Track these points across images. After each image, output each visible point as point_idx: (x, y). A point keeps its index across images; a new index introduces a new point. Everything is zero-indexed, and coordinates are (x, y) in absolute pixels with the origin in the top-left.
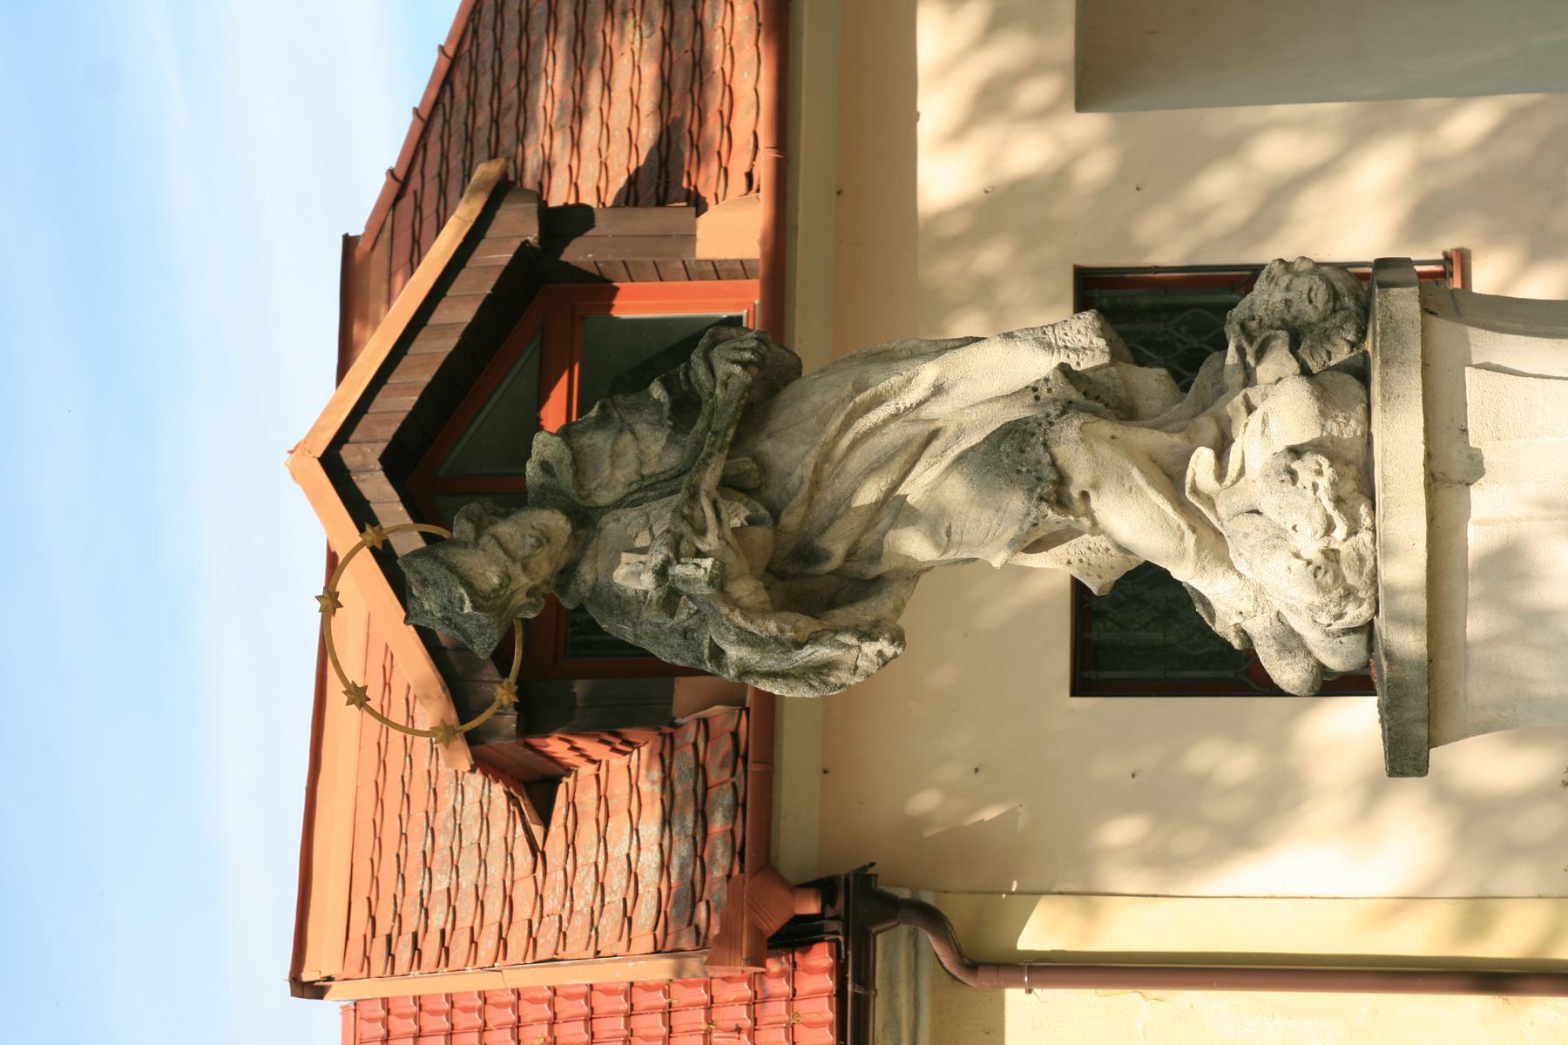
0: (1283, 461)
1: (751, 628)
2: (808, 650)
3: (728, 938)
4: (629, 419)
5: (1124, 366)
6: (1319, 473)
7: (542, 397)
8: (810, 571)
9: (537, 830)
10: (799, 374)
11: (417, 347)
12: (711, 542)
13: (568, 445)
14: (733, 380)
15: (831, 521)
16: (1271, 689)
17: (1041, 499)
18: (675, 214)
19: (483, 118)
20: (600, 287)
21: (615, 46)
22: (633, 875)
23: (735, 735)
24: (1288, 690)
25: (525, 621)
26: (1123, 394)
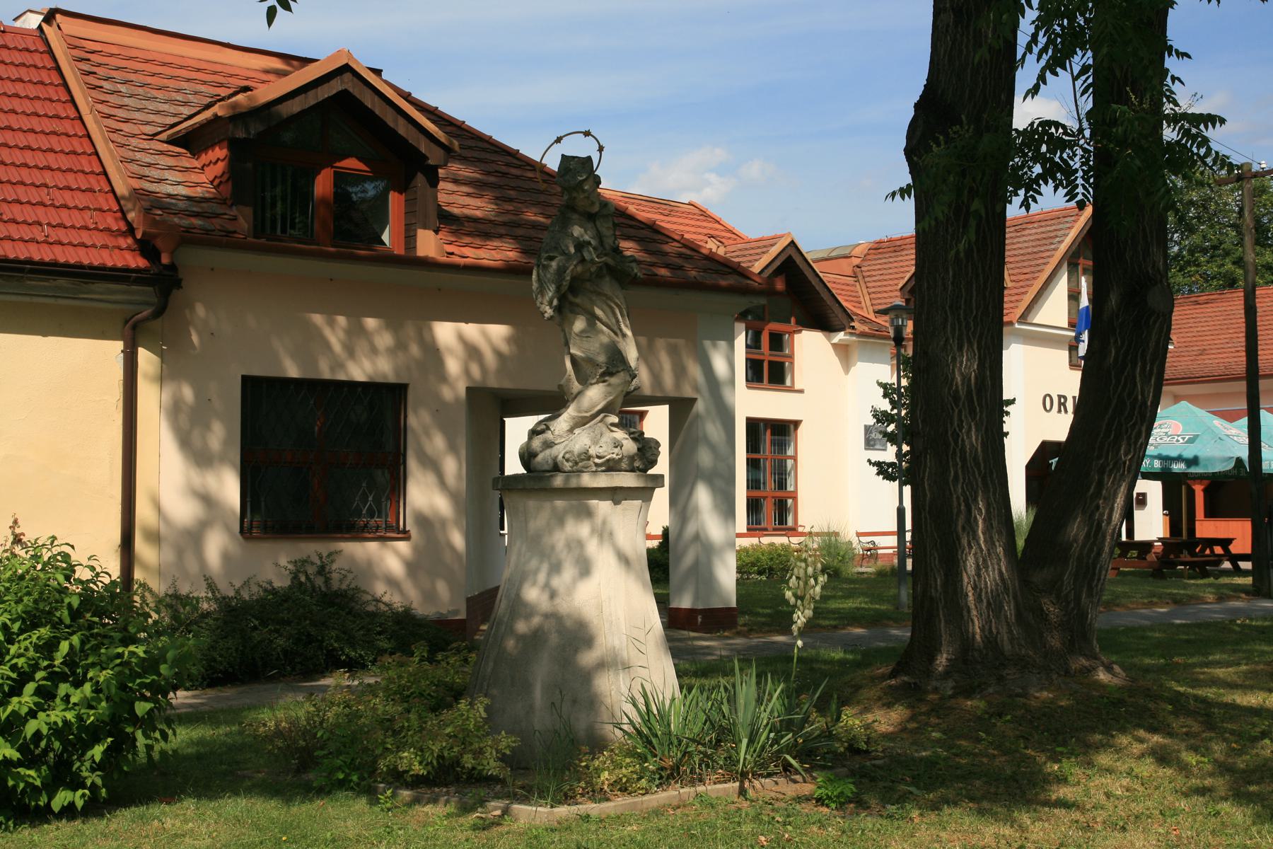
7: (360, 159)
22: (160, 181)
23: (235, 232)
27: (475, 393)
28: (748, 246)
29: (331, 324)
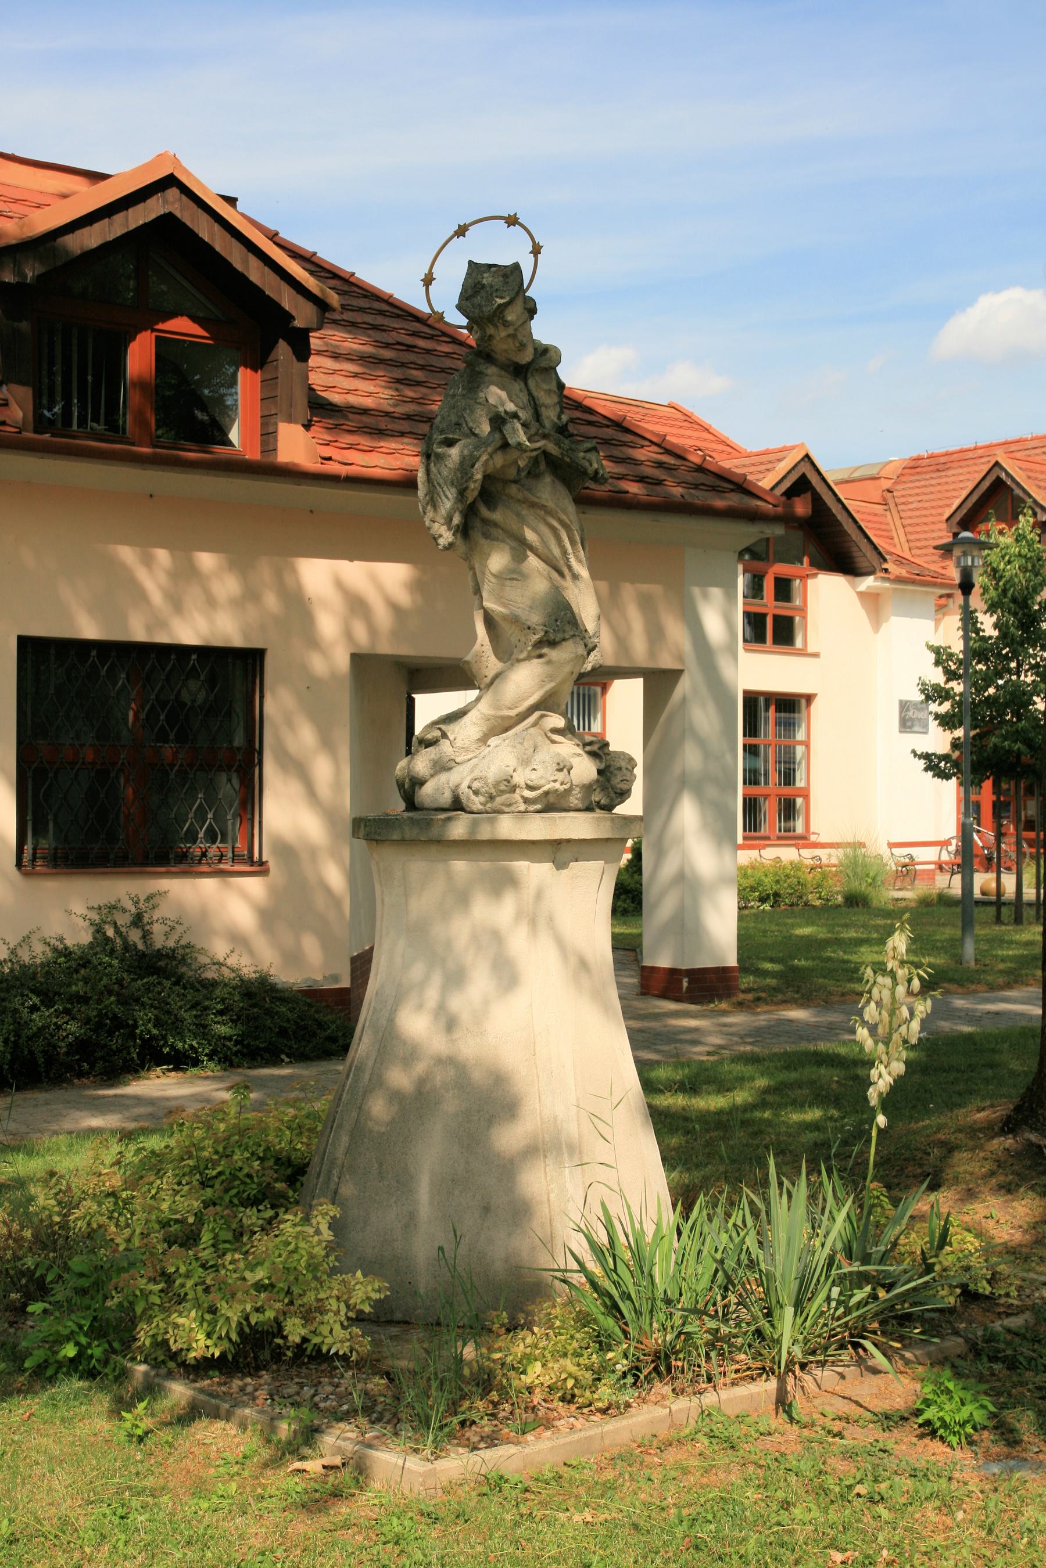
6: (562, 784)
7: (194, 319)
17: (546, 632)
20: (259, 360)
28: (747, 461)
29: (148, 561)
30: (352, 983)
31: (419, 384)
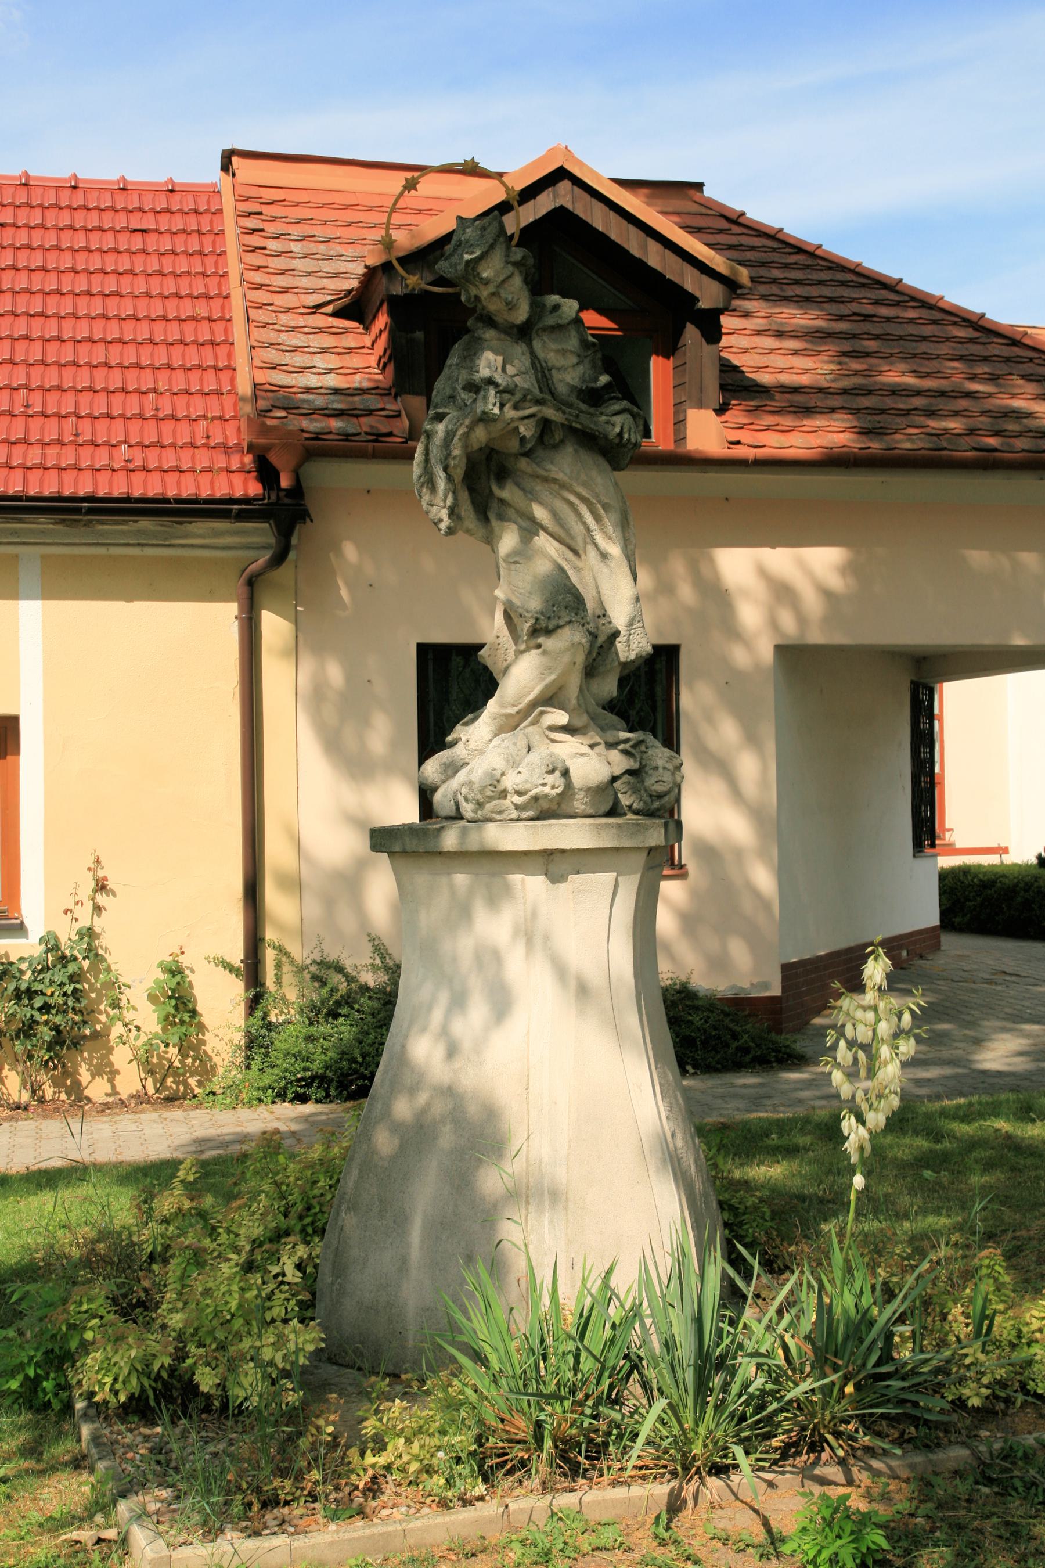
0: (560, 765)
1: (456, 439)
2: (443, 475)
3: (265, 430)
4: (586, 361)
5: (618, 670)
6: (553, 787)
7: (601, 311)
8: (492, 477)
9: (329, 309)
10: (615, 469)
11: (633, 230)
12: (510, 413)
13: (570, 323)
14: (610, 427)
15: (523, 489)
16: (422, 759)
17: (537, 619)
18: (715, 396)
19: (776, 273)
20: (670, 348)
21: (820, 357)
22: (302, 370)
24: (424, 766)
25: (458, 295)
26: (601, 669)
27: (792, 656)
30: (784, 989)
31: (867, 354)
